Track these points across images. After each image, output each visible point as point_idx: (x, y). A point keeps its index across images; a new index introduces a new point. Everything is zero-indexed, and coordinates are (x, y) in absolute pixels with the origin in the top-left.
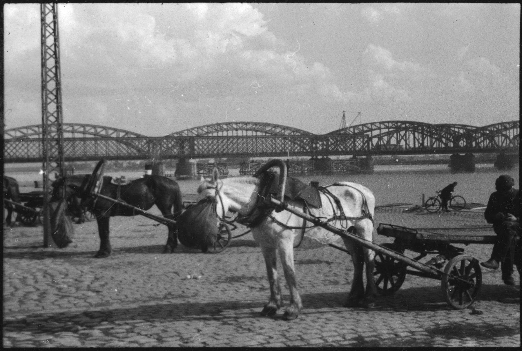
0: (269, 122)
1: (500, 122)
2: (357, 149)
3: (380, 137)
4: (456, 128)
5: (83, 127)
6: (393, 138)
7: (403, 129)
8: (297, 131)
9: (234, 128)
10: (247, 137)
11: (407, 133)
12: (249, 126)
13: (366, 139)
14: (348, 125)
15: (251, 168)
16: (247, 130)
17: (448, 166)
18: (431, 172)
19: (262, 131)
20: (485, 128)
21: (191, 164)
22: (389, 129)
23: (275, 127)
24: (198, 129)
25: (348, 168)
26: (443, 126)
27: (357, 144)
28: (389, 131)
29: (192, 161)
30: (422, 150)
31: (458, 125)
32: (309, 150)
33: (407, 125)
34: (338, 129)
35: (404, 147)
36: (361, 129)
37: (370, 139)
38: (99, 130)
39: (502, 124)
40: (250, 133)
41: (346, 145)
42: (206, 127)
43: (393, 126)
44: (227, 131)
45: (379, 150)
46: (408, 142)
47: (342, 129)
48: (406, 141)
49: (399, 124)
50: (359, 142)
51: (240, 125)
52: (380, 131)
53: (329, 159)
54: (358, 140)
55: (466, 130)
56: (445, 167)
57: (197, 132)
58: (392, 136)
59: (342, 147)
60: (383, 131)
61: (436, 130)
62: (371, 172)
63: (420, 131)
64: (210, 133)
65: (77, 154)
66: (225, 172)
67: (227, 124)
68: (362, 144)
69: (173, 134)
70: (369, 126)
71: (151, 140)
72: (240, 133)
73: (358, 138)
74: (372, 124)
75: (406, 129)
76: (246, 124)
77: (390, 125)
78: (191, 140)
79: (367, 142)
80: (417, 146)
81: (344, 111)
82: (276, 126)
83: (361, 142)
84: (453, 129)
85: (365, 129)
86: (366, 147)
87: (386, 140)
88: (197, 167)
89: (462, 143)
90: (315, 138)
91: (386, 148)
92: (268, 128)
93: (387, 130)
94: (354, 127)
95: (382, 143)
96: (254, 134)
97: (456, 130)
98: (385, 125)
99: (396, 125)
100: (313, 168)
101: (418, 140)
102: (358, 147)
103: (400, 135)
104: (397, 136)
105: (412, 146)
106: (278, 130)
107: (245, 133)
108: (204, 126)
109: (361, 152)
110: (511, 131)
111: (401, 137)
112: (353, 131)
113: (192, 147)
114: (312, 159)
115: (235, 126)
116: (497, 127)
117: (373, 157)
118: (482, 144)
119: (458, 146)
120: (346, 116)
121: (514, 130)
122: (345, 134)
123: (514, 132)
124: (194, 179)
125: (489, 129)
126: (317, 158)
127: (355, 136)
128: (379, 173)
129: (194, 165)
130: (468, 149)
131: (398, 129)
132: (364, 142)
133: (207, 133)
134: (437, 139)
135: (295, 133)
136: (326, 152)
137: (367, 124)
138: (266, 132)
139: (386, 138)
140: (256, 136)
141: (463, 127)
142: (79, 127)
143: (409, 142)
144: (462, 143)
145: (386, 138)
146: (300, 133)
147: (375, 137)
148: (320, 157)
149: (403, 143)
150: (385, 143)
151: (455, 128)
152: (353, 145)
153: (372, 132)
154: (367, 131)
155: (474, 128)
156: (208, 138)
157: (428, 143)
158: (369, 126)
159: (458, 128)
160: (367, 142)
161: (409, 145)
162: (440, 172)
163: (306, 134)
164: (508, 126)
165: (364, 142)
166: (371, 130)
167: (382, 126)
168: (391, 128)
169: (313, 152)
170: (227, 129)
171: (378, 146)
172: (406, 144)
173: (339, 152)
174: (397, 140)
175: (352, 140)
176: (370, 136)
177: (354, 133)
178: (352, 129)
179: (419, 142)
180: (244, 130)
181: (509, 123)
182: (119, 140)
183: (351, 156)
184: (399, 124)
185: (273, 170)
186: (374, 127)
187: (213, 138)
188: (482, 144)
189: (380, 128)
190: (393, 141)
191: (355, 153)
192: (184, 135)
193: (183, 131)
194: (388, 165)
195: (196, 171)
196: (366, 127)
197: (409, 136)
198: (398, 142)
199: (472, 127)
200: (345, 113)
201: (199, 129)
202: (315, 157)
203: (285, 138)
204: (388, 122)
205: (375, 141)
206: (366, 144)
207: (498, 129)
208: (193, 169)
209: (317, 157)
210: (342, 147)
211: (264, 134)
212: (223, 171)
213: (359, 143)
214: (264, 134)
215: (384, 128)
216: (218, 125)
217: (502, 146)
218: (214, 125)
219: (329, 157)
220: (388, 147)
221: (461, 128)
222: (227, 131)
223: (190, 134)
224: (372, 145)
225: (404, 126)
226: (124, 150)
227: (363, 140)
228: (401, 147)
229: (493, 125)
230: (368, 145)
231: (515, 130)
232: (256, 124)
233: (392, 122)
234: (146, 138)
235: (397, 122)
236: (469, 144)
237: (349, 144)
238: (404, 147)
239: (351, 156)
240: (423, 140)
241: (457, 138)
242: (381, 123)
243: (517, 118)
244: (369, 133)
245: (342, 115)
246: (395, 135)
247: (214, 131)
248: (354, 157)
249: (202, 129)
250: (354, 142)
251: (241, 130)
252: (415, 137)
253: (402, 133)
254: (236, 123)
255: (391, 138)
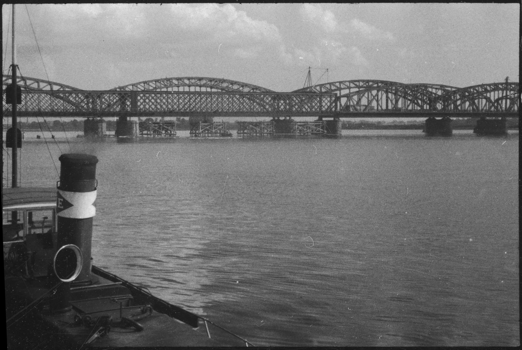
0: (225, 78)
1: (480, 84)
2: (324, 109)
3: (348, 96)
4: (434, 88)
5: (38, 82)
6: (364, 98)
7: (374, 88)
8: (257, 88)
9: (186, 84)
10: (200, 93)
11: (380, 93)
12: (203, 82)
13: (334, 99)
14: (313, 84)
15: (202, 129)
16: (200, 86)
17: (423, 132)
18: (407, 138)
19: (217, 88)
20: (466, 89)
21: (131, 123)
22: (359, 88)
23: (243, 86)
24: (144, 83)
25: (312, 131)
26: (418, 86)
27: (324, 104)
28: (359, 91)
29: (135, 119)
30: (396, 113)
31: (437, 85)
32: (270, 109)
33: (380, 84)
34: (302, 87)
35: (376, 108)
36: (329, 88)
37: (338, 99)
38: (29, 82)
39: (482, 86)
40: (203, 89)
41: (311, 104)
42: (154, 82)
43: (365, 85)
44: (178, 87)
45: (346, 112)
46: (380, 103)
47: (307, 88)
48: (377, 101)
49: (371, 83)
50: (326, 101)
51: (193, 81)
52: (350, 91)
53: (292, 121)
54: (324, 99)
55: (445, 90)
56: (420, 132)
57: (144, 87)
58: (363, 95)
59: (306, 107)
60: (352, 90)
61: (412, 91)
62: (341, 137)
63: (394, 92)
64: (158, 88)
65: (44, 108)
66: (172, 132)
67: (178, 79)
68: (329, 104)
69: (116, 88)
70: (338, 84)
71: (88, 95)
72: (192, 89)
73: (324, 98)
74: (340, 82)
75: (378, 89)
76: (200, 79)
77: (361, 84)
78: (134, 95)
79: (335, 101)
80: (390, 107)
81: (310, 68)
82: (233, 83)
83: (328, 101)
84: (430, 90)
85: (333, 88)
86: (333, 107)
87: (356, 100)
88: (140, 126)
89: (439, 106)
90: (277, 96)
91: (356, 109)
92: (225, 85)
93: (357, 90)
94: (321, 86)
95: (352, 104)
96: (209, 90)
97: (434, 91)
98: (355, 85)
99: (367, 84)
100: (273, 131)
101: (391, 101)
102: (324, 107)
103: (372, 95)
104: (368, 95)
105: (384, 107)
106: (235, 87)
107: (198, 89)
108: (152, 81)
109: (327, 113)
110: (492, 93)
111: (372, 97)
112: (319, 90)
113: (134, 103)
114: (274, 120)
115: (187, 82)
116: (477, 89)
117: (342, 119)
118: (150, 108)
119: (435, 109)
120: (311, 72)
121: (494, 93)
122: (311, 92)
123: (503, 93)
124: (136, 142)
125: (485, 87)
126: (278, 119)
127: (321, 95)
128: (347, 137)
129: (136, 123)
130: (444, 113)
131: (369, 89)
132: (332, 101)
133: (155, 88)
134: (412, 101)
135: (255, 90)
136: (290, 113)
137: (335, 83)
138: (222, 89)
139: (356, 98)
140: (200, 91)
141: (442, 87)
142: (32, 82)
143: (381, 103)
144: (439, 106)
145: (356, 98)
146: (259, 90)
147: (344, 96)
148: (282, 118)
149: (374, 104)
150: (355, 103)
151: (432, 88)
152: (318, 104)
153: (340, 91)
154: (335, 90)
155: (453, 89)
156: (156, 93)
157: (482, 101)
158: (338, 84)
159: (436, 89)
160: (335, 101)
161: (381, 107)
162: (415, 137)
163: (267, 92)
164: (488, 88)
165: (332, 101)
166: (340, 89)
167: (352, 85)
168: (362, 87)
169: (276, 112)
170: (178, 84)
171: (347, 107)
172: (378, 105)
173: (303, 112)
174: (368, 100)
175: (318, 99)
176: (338, 95)
177: (321, 92)
178: (318, 88)
179: (392, 103)
180: (208, 87)
181: (489, 85)
182: (52, 93)
183: (316, 118)
184: (371, 83)
185: (322, 108)
186: (342, 86)
187: (161, 93)
188: (150, 108)
189: (349, 88)
190: (364, 101)
191: (321, 114)
192: (127, 89)
193: (127, 86)
194: (358, 129)
195: (138, 131)
196: (334, 85)
197: (382, 95)
198: (370, 102)
199: (452, 87)
200: (311, 69)
201: (145, 84)
202: (276, 118)
203: (242, 95)
204: (358, 81)
205: (344, 101)
206: (334, 104)
207: (478, 91)
208: (135, 129)
209: (278, 118)
210: (306, 107)
211: (220, 91)
212: (171, 132)
213: (326, 102)
214: (220, 91)
215: (355, 87)
216: (168, 80)
217: (417, 109)
218: (163, 80)
219: (293, 118)
220: (358, 108)
221: (439, 89)
222: (178, 87)
223: (135, 89)
224: (341, 105)
225: (376, 85)
226: (59, 104)
227: (331, 99)
228: (372, 108)
229: (473, 87)
230: (336, 106)
231: (496, 92)
232: (211, 80)
233: (363, 81)
234: (82, 92)
235: (368, 81)
236: (445, 107)
237: (315, 103)
238: (376, 108)
239: (316, 118)
240: (397, 101)
241: (433, 100)
242: (350, 82)
243: (515, 78)
244: (338, 92)
245: (308, 70)
246: (366, 95)
247: (162, 86)
248: (320, 119)
249: (148, 84)
250: (320, 102)
251: (194, 86)
252: (387, 97)
253: (374, 92)
254: (189, 79)
255: (362, 97)
